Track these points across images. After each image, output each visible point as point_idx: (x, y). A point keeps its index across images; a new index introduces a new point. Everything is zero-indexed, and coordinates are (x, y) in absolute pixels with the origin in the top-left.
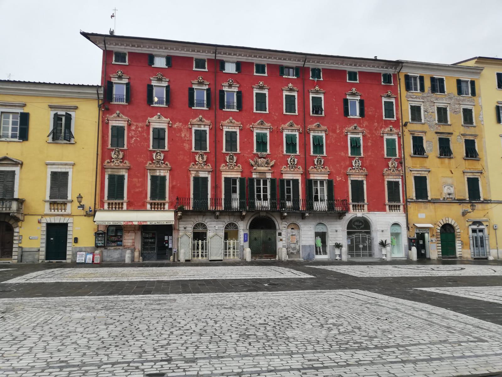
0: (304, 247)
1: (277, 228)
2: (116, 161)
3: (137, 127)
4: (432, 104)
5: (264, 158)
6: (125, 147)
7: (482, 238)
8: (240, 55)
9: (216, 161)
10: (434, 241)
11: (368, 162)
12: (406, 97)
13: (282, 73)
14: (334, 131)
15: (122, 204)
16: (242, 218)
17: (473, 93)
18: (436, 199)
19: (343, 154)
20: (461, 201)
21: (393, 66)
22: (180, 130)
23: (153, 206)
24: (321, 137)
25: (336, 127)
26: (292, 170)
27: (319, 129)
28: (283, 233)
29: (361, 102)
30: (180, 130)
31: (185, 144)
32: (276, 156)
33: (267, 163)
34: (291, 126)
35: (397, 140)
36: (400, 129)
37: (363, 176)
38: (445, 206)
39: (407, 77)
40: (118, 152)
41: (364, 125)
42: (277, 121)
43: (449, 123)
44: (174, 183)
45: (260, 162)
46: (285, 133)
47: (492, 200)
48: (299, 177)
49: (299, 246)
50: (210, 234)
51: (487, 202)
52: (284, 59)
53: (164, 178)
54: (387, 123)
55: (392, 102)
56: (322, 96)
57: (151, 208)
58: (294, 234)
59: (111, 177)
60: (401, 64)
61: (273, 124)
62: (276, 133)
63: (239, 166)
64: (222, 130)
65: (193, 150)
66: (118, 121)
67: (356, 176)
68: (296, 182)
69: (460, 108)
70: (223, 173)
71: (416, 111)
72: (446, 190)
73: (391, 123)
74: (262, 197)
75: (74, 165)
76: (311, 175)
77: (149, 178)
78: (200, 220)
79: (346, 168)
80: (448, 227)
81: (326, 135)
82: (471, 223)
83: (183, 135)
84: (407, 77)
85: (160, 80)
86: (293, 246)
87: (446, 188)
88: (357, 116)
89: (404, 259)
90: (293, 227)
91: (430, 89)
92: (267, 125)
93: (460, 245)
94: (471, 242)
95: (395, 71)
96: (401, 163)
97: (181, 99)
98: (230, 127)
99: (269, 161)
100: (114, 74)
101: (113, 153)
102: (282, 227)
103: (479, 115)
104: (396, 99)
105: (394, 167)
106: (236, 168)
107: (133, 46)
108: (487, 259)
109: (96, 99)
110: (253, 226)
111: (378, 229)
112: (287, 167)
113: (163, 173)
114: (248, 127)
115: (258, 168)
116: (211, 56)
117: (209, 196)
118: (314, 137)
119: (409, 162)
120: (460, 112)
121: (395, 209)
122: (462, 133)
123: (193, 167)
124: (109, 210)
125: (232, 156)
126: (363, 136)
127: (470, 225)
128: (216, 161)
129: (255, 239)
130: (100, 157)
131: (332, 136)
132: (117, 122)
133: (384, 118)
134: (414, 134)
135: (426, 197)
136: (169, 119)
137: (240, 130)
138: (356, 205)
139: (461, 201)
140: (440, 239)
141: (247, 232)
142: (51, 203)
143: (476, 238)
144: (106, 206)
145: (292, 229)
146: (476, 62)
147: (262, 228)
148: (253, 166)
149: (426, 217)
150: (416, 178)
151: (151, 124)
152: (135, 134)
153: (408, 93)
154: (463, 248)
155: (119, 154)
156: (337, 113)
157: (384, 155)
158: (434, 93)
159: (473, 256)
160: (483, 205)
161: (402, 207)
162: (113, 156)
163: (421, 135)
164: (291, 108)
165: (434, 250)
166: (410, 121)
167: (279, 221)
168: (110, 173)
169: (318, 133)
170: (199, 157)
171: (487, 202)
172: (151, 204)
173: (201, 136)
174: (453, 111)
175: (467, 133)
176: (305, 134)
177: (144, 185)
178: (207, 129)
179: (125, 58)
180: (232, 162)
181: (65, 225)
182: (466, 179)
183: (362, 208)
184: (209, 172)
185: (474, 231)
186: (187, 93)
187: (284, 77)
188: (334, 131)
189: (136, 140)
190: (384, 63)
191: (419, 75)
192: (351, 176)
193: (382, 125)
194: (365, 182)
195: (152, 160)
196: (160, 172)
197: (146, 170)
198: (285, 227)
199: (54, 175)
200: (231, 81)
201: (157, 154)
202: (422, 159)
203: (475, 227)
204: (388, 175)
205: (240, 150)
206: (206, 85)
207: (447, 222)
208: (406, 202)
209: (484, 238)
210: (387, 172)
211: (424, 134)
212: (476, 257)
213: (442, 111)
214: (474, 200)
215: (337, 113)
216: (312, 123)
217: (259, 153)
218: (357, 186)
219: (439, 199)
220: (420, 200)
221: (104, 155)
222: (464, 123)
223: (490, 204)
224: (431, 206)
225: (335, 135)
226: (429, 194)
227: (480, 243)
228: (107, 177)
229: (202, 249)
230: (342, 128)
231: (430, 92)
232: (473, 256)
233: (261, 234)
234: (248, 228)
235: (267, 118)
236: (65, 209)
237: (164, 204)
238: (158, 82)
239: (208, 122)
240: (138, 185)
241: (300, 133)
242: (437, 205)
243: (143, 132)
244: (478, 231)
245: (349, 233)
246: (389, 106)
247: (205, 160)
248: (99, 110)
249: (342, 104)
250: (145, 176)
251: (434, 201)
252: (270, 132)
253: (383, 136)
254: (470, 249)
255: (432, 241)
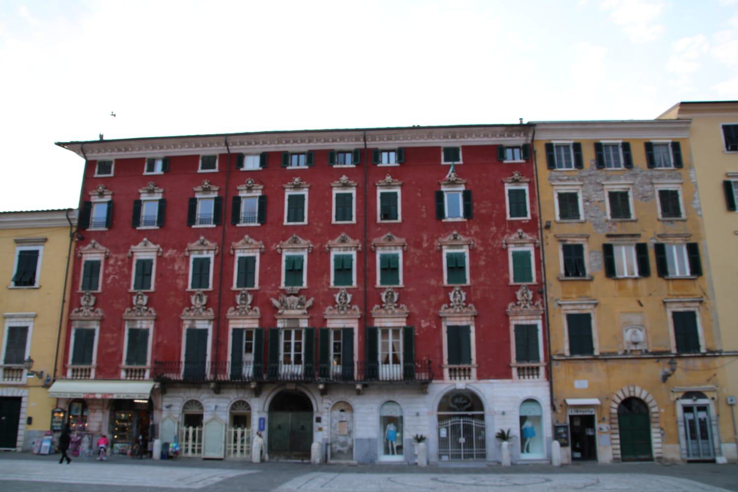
0: (360, 440)
1: (315, 409)
2: (85, 310)
3: (117, 260)
4: (599, 188)
5: (295, 295)
6: (100, 290)
7: (703, 423)
8: (264, 143)
9: (220, 303)
10: (605, 430)
11: (479, 293)
12: (550, 179)
13: (333, 162)
14: (418, 245)
15: (90, 370)
16: (257, 393)
17: (678, 163)
18: (609, 354)
19: (433, 282)
20: (658, 355)
21: (520, 131)
22: (173, 260)
23: (129, 374)
24: (396, 257)
25: (422, 239)
26: (342, 312)
27: (390, 243)
28: (325, 418)
29: (467, 195)
30: (173, 260)
31: (178, 281)
32: (316, 291)
33: (300, 303)
34: (343, 241)
35: (533, 253)
36: (537, 235)
37: (469, 319)
38: (628, 366)
39: (549, 147)
40: (89, 296)
41: (473, 232)
42: (320, 234)
43: (633, 217)
44: (160, 340)
45: (288, 302)
46: (334, 253)
47: (725, 349)
48: (354, 325)
49: (353, 441)
50: (206, 417)
51: (713, 354)
52: (333, 141)
53: (146, 332)
54: (513, 226)
55: (523, 191)
56: (398, 191)
57: (127, 376)
58: (344, 419)
59: (79, 332)
60: (532, 128)
61: (313, 241)
62: (319, 256)
63: (256, 311)
64: (233, 256)
65: (190, 288)
66: (94, 254)
67: (456, 319)
68: (349, 332)
69: (654, 191)
70: (231, 322)
71: (568, 204)
72: (628, 336)
73: (520, 224)
74: (292, 359)
75: (35, 317)
76: (376, 320)
77: (126, 332)
78: (193, 395)
79: (438, 306)
80: (635, 403)
81: (404, 253)
82: (680, 395)
83: (176, 267)
84: (549, 147)
85: (151, 192)
86: (342, 439)
87: (630, 332)
88: (460, 218)
89: (544, 462)
90: (343, 408)
91: (593, 163)
92: (303, 242)
93: (659, 435)
94: (682, 430)
95: (527, 140)
96: (541, 293)
97: (178, 214)
98: (246, 251)
99: (304, 299)
100: (94, 191)
101: (82, 299)
102: (322, 406)
103: (690, 200)
104: (531, 185)
105: (527, 300)
106: (250, 313)
107: (120, 150)
108: (713, 461)
109: (67, 227)
110: (276, 406)
111: (496, 409)
112: (334, 308)
113: (147, 324)
114: (273, 248)
115: (286, 312)
116: (222, 150)
117: (209, 358)
118: (383, 257)
119: (554, 290)
120: (653, 197)
121: (530, 372)
122: (659, 232)
123: (187, 314)
124: (72, 379)
125: (245, 294)
126: (470, 250)
127: (678, 399)
128: (220, 303)
129: (280, 427)
130: (67, 305)
131: (415, 253)
132: (93, 255)
133: (508, 218)
134: (565, 241)
135: (591, 350)
136: (158, 246)
137: (262, 254)
138: (455, 369)
139: (658, 355)
140: (617, 426)
141: (265, 416)
142: (7, 370)
143: (692, 422)
144: (69, 374)
145: (342, 411)
146: (680, 111)
147: (291, 410)
148: (277, 309)
149: (585, 388)
150: (570, 318)
151: (135, 254)
152: (113, 270)
153: (553, 173)
154: (663, 442)
155: (90, 299)
156: (424, 216)
157: (508, 280)
158: (602, 168)
159: (685, 457)
160: (706, 360)
161: (542, 371)
162: (83, 303)
163: (578, 241)
164: (343, 213)
165: (608, 446)
166: (558, 218)
167: (318, 397)
168: (77, 326)
169: (390, 249)
170: (196, 299)
171: (713, 354)
172: (127, 371)
173: (201, 265)
174: (640, 196)
175: (670, 232)
176: (366, 255)
177: (119, 342)
178: (211, 256)
179: (110, 168)
180: (245, 304)
181: (18, 400)
182: (670, 315)
183: (467, 373)
184: (210, 320)
185: (687, 409)
186: (186, 204)
187: (335, 166)
188: (418, 245)
189: (114, 278)
190: (504, 128)
191: (572, 142)
192: (448, 319)
193: (505, 229)
194: (473, 329)
195: (132, 306)
196: (141, 324)
197: (123, 321)
198: (327, 408)
199: (12, 330)
200: (250, 182)
201: (138, 297)
202: (582, 283)
203: (688, 402)
204: (516, 314)
205: (260, 284)
206: (214, 191)
207: (632, 394)
208: (549, 359)
209: (708, 423)
210: (514, 309)
211: (585, 239)
212: (691, 458)
213: (619, 198)
214: (688, 351)
215: (424, 216)
216: (380, 234)
217: (289, 288)
218: (458, 335)
219: (615, 353)
220: (577, 357)
221: (73, 302)
222: (663, 216)
223: (720, 359)
224: (599, 367)
225: (419, 252)
226: (596, 345)
227: (699, 431)
228: (73, 332)
229: (194, 440)
230: (432, 239)
231: (595, 168)
232: (685, 457)
233: (287, 418)
234: (266, 408)
235: (303, 232)
236: (21, 378)
237: (144, 371)
238: (150, 195)
239: (213, 245)
240: (112, 343)
241: (359, 253)
242: (610, 364)
243: (123, 266)
244: (695, 409)
245: (441, 418)
246: (516, 196)
247: (204, 302)
248: (72, 240)
249: (431, 199)
250: (121, 330)
251: (605, 358)
252: (309, 254)
253: (507, 248)
254: (679, 442)
255: (601, 429)
